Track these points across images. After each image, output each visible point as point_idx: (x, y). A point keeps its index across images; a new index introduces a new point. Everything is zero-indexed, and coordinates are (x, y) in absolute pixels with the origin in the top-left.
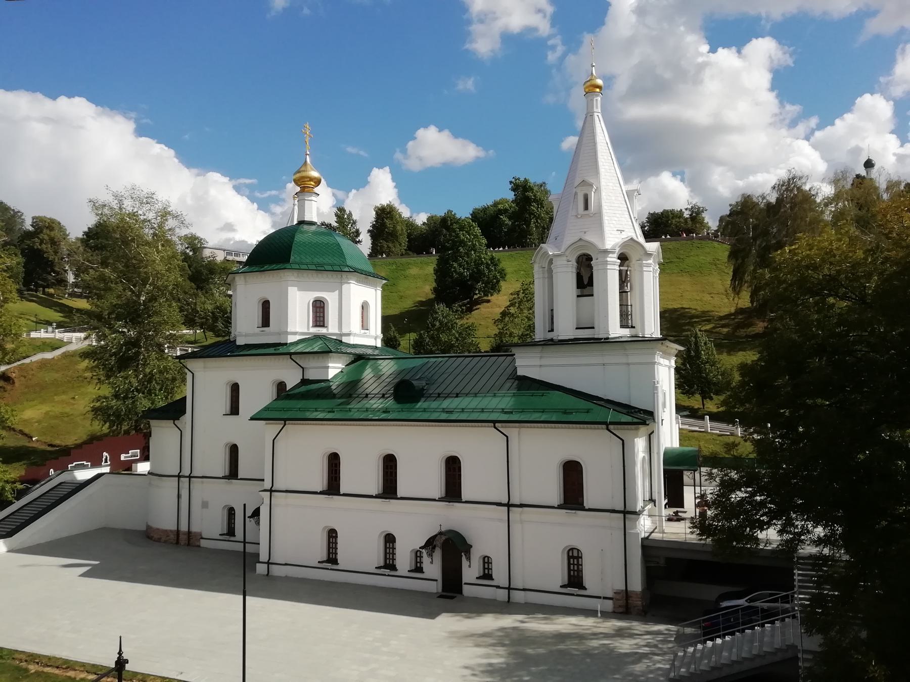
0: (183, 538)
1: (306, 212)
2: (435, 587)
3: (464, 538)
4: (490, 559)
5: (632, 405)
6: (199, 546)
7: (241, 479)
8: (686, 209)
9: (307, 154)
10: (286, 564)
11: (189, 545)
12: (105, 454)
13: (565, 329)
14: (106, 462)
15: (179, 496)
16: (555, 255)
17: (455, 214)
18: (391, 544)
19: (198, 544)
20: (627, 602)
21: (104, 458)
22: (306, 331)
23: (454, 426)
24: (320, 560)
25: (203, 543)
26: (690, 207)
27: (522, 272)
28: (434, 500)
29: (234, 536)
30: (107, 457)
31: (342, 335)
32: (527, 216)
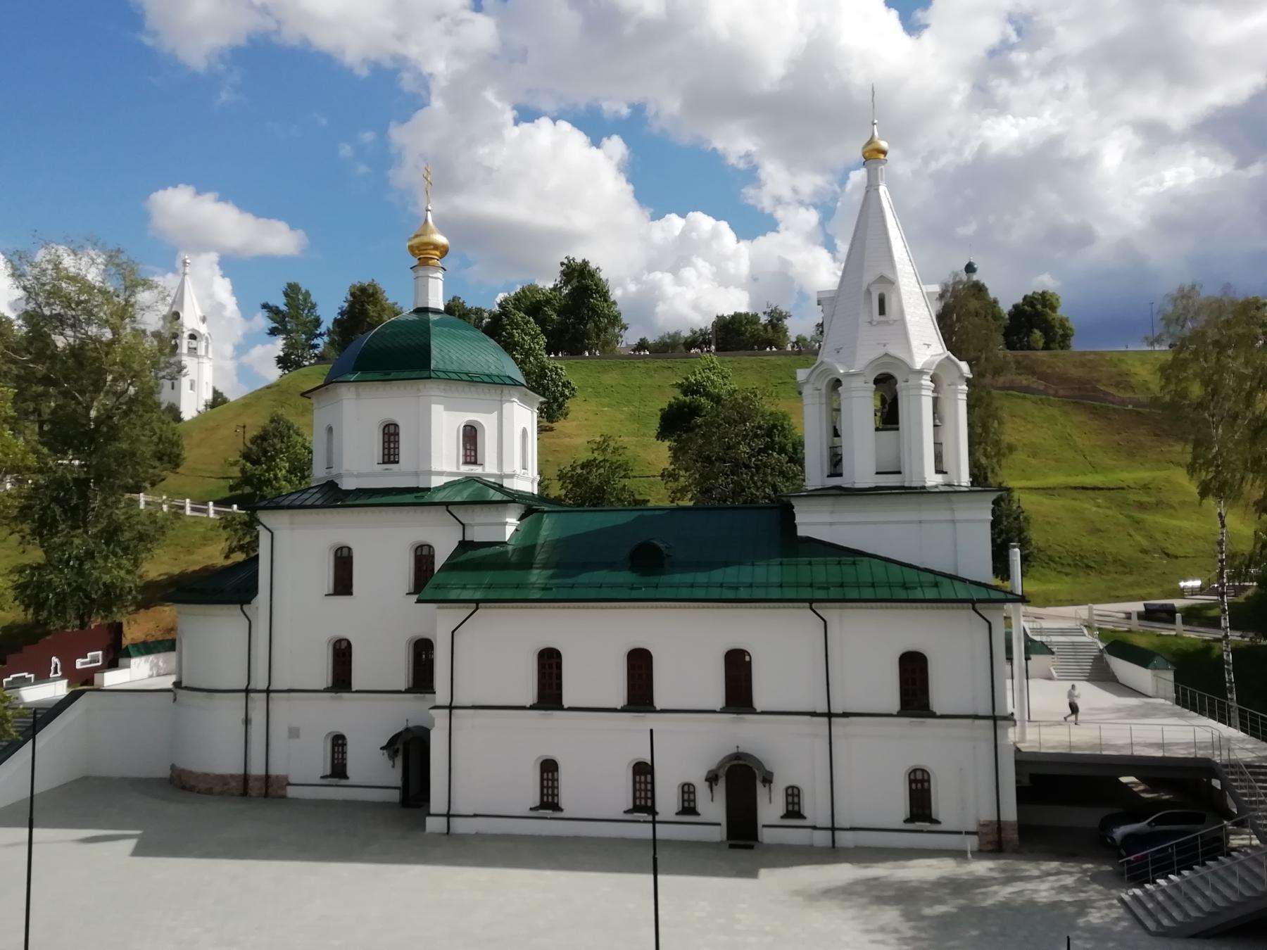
0: (255, 788)
1: (430, 294)
2: (718, 834)
4: (691, 787)
5: (960, 575)
6: (284, 797)
7: (357, 692)
8: (765, 313)
9: (427, 210)
10: (475, 816)
11: (266, 795)
12: (55, 660)
13: (861, 472)
14: (56, 672)
15: (247, 721)
16: (848, 375)
17: (464, 302)
18: (550, 775)
19: (283, 793)
21: (53, 666)
22: (454, 470)
23: (583, 608)
24: (533, 806)
25: (292, 792)
26: (769, 310)
27: (590, 390)
28: (714, 712)
29: (346, 777)
30: (57, 665)
31: (502, 476)
32: (586, 312)
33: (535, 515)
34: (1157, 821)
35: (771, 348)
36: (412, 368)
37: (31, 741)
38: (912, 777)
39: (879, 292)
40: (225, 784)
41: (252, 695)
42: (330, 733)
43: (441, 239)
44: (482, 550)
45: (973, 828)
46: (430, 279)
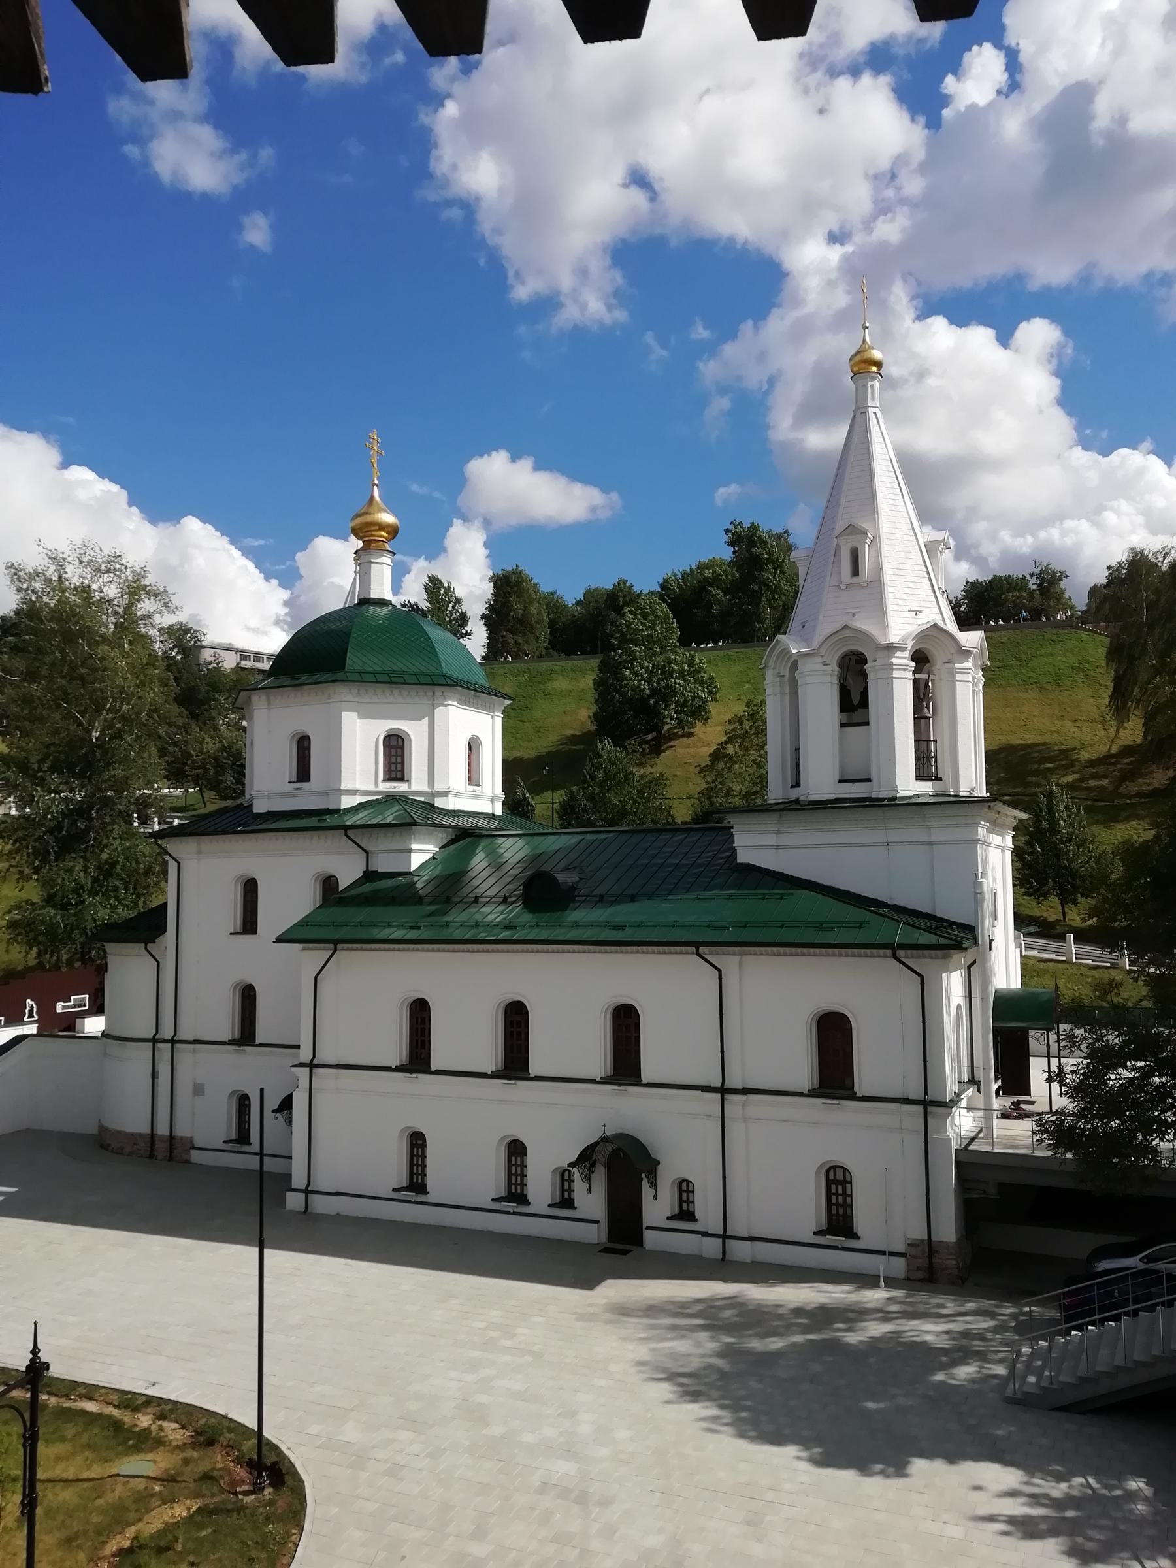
0: (161, 1147)
2: (595, 1234)
3: (637, 1139)
6: (188, 1162)
7: (261, 1045)
9: (374, 485)
10: (337, 1194)
11: (170, 1159)
15: (154, 1075)
20: (931, 1263)
21: (28, 1008)
22: (372, 787)
23: (423, 950)
25: (196, 1157)
26: (1038, 571)
30: (32, 1007)
31: (433, 795)
33: (468, 840)
34: (1149, 1259)
35: (996, 622)
36: (322, 669)
37: (971, 1148)
38: (831, 1177)
39: (850, 546)
40: (135, 1144)
41: (178, 1046)
42: (235, 1092)
43: (387, 518)
44: (383, 881)
45: (900, 1248)
46: (372, 565)
